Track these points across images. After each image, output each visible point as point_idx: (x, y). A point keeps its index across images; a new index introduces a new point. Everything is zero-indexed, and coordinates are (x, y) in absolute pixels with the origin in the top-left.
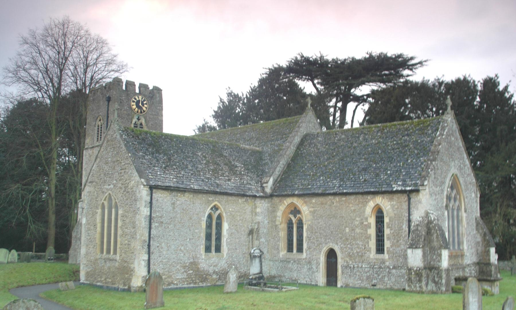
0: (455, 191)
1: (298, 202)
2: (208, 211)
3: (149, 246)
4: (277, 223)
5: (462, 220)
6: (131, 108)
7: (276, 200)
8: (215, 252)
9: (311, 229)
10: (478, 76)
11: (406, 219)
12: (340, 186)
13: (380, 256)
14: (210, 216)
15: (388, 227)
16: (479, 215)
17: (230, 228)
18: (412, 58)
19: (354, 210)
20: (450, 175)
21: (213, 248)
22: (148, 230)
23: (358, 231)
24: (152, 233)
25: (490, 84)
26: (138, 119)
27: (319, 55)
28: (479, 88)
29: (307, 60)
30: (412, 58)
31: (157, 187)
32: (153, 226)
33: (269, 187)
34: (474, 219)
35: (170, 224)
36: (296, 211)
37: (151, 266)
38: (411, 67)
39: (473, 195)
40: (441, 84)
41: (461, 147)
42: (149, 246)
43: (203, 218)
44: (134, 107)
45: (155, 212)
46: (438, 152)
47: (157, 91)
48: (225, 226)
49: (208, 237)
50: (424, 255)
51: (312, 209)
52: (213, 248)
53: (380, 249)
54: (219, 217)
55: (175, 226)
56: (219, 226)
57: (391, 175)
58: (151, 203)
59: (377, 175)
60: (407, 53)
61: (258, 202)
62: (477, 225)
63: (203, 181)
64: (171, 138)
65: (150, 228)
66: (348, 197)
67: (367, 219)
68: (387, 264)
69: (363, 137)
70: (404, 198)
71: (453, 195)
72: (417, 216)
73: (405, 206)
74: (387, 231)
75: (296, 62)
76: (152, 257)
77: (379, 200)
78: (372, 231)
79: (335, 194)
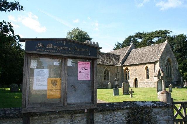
13: (148, 79)
18: (168, 31)
20: (167, 58)
23: (142, 73)
27: (143, 32)
29: (140, 33)
30: (168, 31)
38: (169, 33)
40: (175, 36)
46: (37, 76)
48: (109, 73)
53: (148, 77)
59: (147, 59)
60: (167, 29)
71: (168, 63)
73: (154, 66)
74: (149, 73)
75: (137, 34)
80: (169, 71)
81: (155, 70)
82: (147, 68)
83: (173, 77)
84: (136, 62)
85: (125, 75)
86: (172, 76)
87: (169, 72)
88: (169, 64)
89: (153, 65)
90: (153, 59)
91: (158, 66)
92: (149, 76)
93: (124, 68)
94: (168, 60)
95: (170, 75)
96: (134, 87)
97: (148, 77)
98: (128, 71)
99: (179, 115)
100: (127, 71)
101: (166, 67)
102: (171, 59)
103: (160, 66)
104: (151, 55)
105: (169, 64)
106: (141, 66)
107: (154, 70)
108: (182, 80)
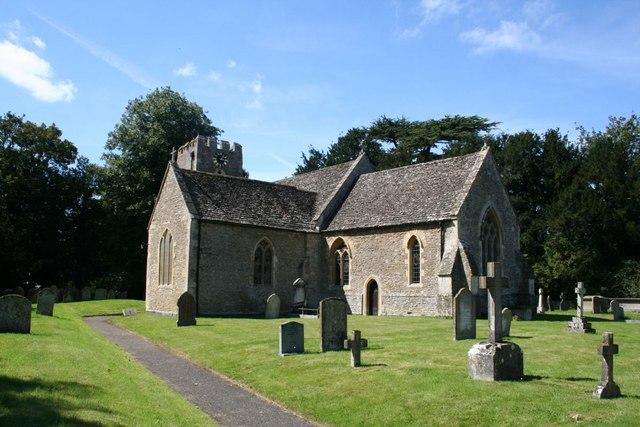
0: (492, 224)
4: (533, 222)
10: (540, 131)
18: (486, 120)
20: (485, 208)
25: (552, 136)
28: (542, 138)
29: (389, 122)
30: (486, 120)
39: (513, 229)
40: (505, 137)
47: (238, 147)
48: (275, 259)
53: (415, 278)
54: (269, 251)
57: (427, 207)
58: (199, 235)
60: (482, 116)
62: (517, 259)
64: (250, 181)
65: (198, 258)
69: (200, 142)
71: (490, 228)
77: (415, 232)
81: (442, 250)
82: (414, 244)
84: (376, 221)
85: (331, 268)
88: (492, 232)
89: (437, 232)
90: (438, 212)
91: (453, 240)
92: (422, 273)
93: (331, 241)
96: (364, 314)
97: (415, 278)
98: (346, 254)
100: (341, 254)
102: (499, 214)
103: (461, 238)
104: (428, 194)
105: (492, 232)
106: (392, 237)
107: (439, 253)
108: (531, 291)
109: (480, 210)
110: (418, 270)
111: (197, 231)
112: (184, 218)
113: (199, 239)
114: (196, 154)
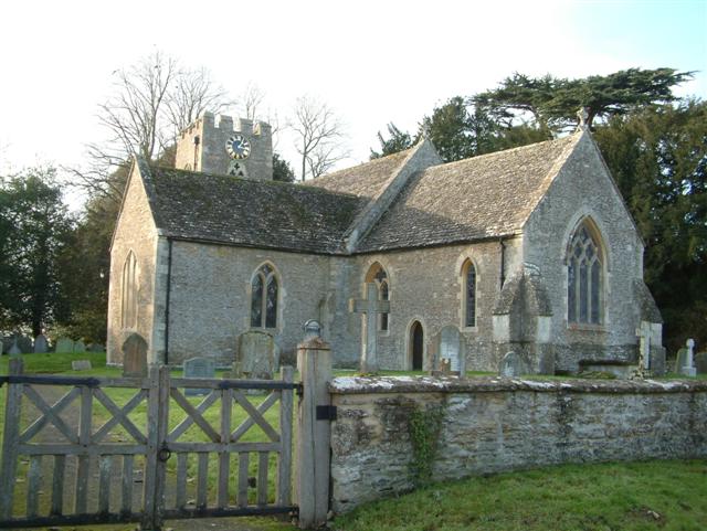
0: (589, 241)
1: (381, 259)
2: (256, 272)
3: (167, 313)
5: (603, 282)
6: (226, 151)
7: (360, 259)
8: (267, 326)
9: (396, 295)
11: (499, 276)
12: (431, 236)
13: (470, 329)
14: (260, 281)
15: (479, 289)
16: (641, 277)
17: (289, 295)
19: (443, 268)
21: (264, 321)
22: (165, 293)
23: (446, 296)
24: (171, 296)
26: (237, 167)
29: (524, 79)
31: (180, 239)
32: (173, 288)
33: (352, 243)
34: (631, 282)
35: (197, 286)
36: (381, 275)
37: (170, 339)
39: (630, 248)
41: (603, 178)
42: (167, 313)
43: (247, 281)
44: (230, 150)
45: (176, 269)
48: (282, 293)
49: (256, 304)
50: (512, 322)
51: (397, 270)
52: (264, 321)
54: (274, 282)
55: (205, 289)
56: (274, 297)
58: (170, 258)
61: (334, 261)
62: (635, 292)
63: (251, 233)
65: (168, 291)
66: (437, 250)
67: (456, 279)
68: (477, 339)
70: (497, 247)
71: (585, 247)
72: (511, 275)
74: (478, 295)
75: (509, 83)
76: (171, 326)
77: (471, 252)
78: (461, 296)
79: (421, 248)
80: (584, 290)
81: (503, 279)
83: (607, 320)
86: (604, 315)
87: (584, 299)
88: (590, 252)
90: (502, 223)
94: (586, 230)
95: (590, 309)
99: (120, 427)
101: (565, 269)
102: (602, 226)
107: (499, 282)
109: (566, 220)
110: (473, 308)
111: (166, 253)
112: (150, 236)
113: (170, 264)
114: (201, 141)
